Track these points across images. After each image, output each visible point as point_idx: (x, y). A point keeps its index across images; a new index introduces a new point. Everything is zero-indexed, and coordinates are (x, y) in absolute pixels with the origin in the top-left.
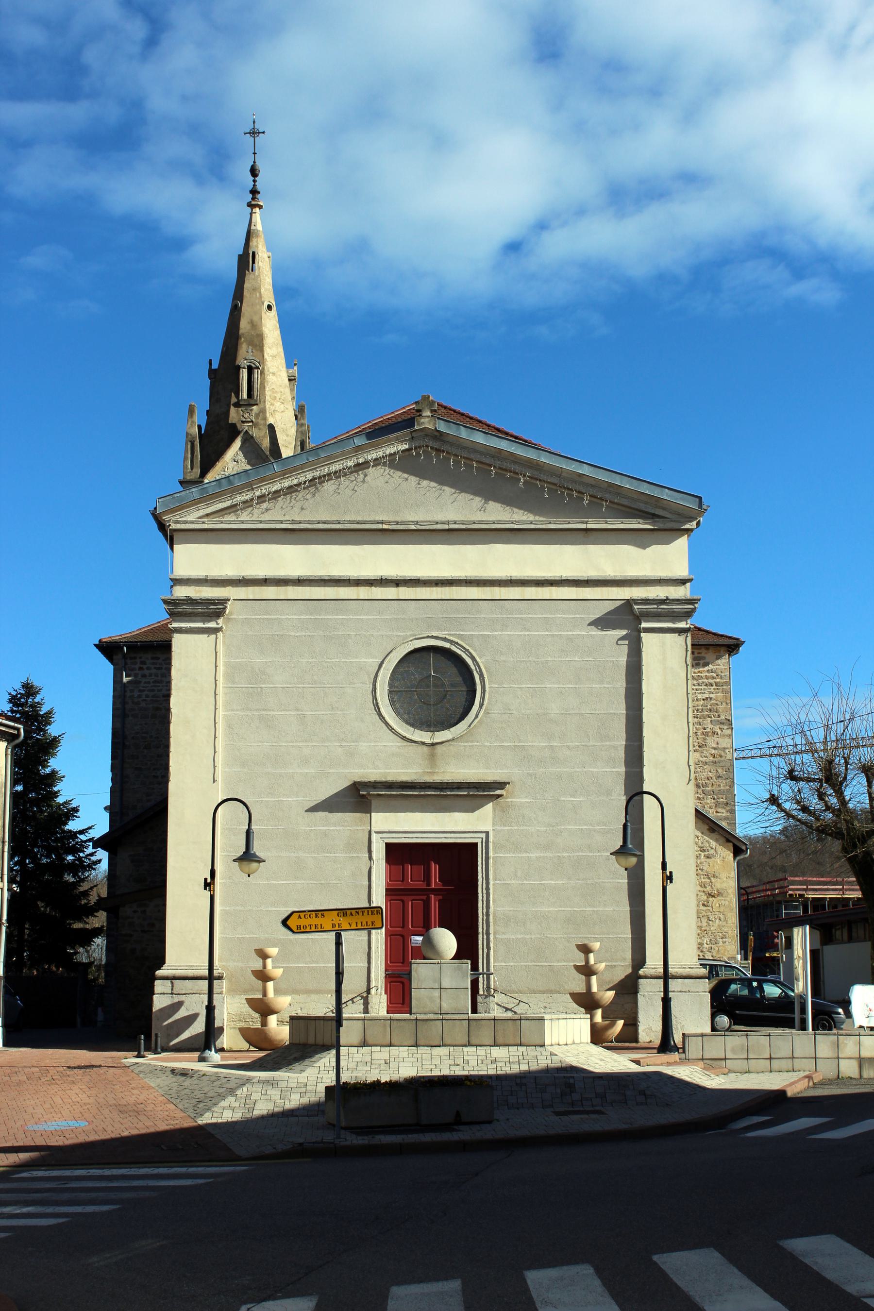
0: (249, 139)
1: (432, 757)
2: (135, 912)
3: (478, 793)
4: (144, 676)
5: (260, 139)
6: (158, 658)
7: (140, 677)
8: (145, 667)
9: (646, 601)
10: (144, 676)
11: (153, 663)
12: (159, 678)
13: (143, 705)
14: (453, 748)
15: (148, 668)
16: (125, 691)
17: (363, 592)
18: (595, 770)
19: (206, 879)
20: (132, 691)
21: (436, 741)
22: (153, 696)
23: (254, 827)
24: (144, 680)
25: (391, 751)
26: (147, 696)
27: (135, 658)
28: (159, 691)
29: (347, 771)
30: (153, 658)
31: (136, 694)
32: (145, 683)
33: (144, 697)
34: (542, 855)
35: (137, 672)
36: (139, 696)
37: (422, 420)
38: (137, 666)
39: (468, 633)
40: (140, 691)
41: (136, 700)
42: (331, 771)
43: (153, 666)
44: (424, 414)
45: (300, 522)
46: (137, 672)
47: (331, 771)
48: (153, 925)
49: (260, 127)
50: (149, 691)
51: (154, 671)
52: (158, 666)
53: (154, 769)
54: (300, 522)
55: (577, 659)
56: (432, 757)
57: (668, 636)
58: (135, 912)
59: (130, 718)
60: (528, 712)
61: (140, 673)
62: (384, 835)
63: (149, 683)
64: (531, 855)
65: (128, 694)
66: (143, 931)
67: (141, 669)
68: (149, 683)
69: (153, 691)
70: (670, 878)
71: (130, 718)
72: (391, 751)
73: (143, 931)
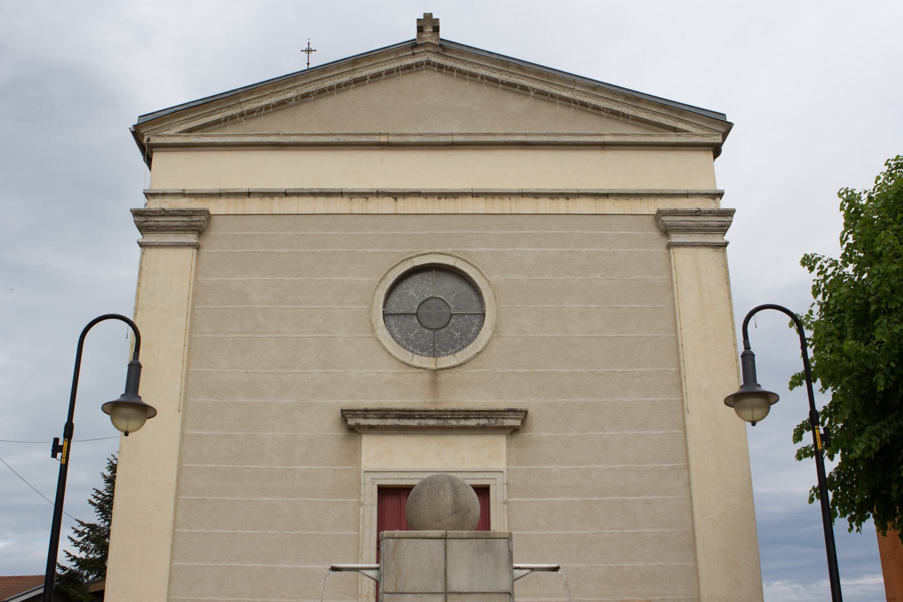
0: (305, 55)
1: (435, 384)
3: (506, 423)
5: (312, 54)
9: (675, 213)
14: (457, 374)
17: (358, 206)
18: (627, 400)
19: (56, 440)
21: (439, 366)
23: (142, 360)
25: (390, 376)
29: (334, 401)
34: (569, 499)
37: (424, 36)
39: (475, 250)
42: (315, 401)
44: (425, 30)
45: (290, 135)
47: (315, 401)
49: (312, 47)
54: (290, 135)
55: (599, 277)
56: (435, 384)
57: (702, 251)
60: (545, 335)
62: (376, 475)
64: (555, 499)
70: (56, 448)
72: (390, 376)
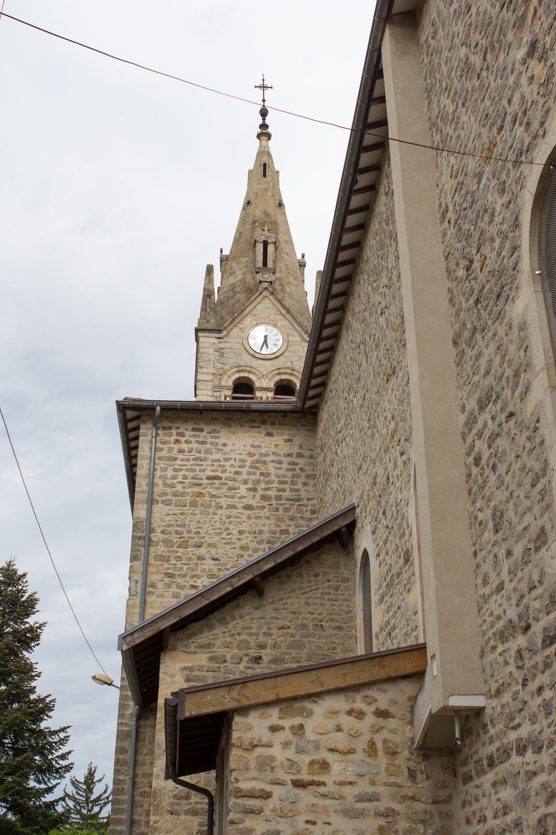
2: (274, 729)
4: (181, 451)
6: (202, 430)
7: (175, 451)
8: (183, 439)
10: (181, 451)
11: (194, 436)
12: (202, 455)
13: (179, 488)
15: (187, 442)
16: (155, 470)
20: (164, 470)
22: (192, 478)
24: (180, 456)
26: (185, 477)
27: (170, 428)
28: (201, 471)
30: (194, 430)
31: (170, 473)
32: (182, 460)
33: (180, 479)
35: (172, 445)
36: (174, 477)
38: (172, 439)
40: (175, 470)
41: (169, 482)
43: (193, 440)
46: (172, 445)
48: (325, 766)
50: (188, 470)
51: (195, 446)
52: (201, 439)
53: (193, 577)
58: (274, 729)
59: (160, 505)
61: (176, 447)
63: (188, 460)
65: (158, 473)
66: (299, 784)
67: (177, 441)
68: (188, 460)
69: (194, 470)
71: (160, 505)
73: (299, 784)
